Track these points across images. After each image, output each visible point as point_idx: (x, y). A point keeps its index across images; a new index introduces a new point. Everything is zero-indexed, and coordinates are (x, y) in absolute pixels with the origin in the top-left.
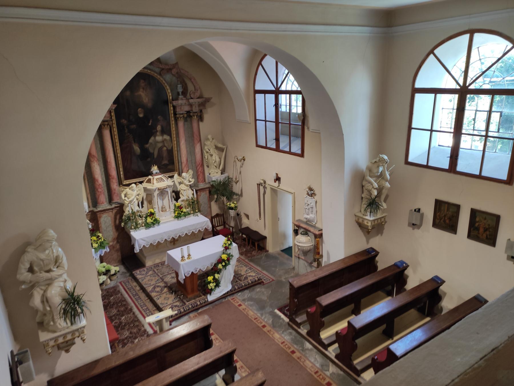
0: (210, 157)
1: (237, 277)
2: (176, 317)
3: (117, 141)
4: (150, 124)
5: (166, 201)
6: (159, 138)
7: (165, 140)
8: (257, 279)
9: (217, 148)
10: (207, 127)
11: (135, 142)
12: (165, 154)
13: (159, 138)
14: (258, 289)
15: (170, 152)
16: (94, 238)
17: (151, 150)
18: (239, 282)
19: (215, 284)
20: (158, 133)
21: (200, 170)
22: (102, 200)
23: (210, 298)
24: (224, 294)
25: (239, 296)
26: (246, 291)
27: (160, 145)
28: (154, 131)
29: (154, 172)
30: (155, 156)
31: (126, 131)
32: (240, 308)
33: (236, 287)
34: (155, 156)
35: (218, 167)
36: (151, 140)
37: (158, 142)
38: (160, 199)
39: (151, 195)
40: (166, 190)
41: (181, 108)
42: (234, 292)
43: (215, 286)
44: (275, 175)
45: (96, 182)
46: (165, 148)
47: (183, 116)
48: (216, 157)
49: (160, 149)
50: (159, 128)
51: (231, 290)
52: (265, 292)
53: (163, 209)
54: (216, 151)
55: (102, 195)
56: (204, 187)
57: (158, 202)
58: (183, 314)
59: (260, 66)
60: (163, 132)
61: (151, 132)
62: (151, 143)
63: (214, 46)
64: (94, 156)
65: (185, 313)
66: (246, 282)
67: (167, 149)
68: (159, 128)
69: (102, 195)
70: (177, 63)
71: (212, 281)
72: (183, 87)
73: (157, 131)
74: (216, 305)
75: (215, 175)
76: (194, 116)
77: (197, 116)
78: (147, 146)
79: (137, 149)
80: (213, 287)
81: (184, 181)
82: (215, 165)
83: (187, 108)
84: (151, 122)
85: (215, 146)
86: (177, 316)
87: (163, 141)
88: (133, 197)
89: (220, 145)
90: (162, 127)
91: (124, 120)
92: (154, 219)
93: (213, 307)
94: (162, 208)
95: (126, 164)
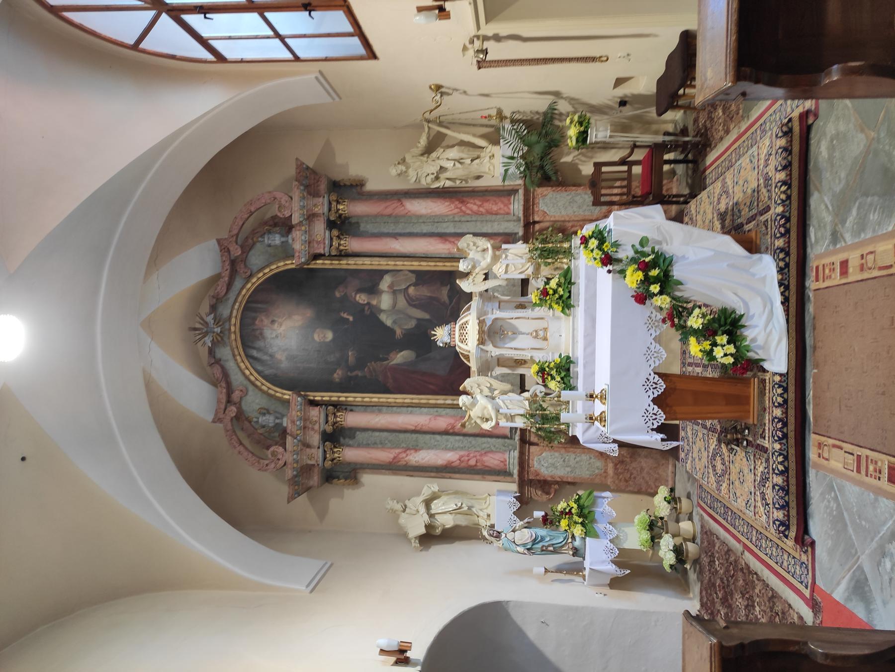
0: (448, 175)
1: (739, 228)
2: (793, 512)
3: (375, 398)
4: (351, 319)
5: (523, 326)
6: (385, 301)
7: (389, 287)
8: (782, 142)
9: (428, 151)
10: (376, 168)
11: (387, 359)
12: (425, 292)
13: (385, 301)
14: (821, 149)
15: (422, 277)
16: (564, 523)
17: (412, 324)
18: (767, 216)
19: (722, 339)
20: (374, 302)
21: (475, 208)
22: (496, 462)
23: (777, 360)
24: (785, 302)
25: (820, 250)
26: (814, 201)
27: (402, 302)
28: (367, 312)
29: (447, 339)
30: (427, 316)
31: (360, 374)
32: (854, 275)
33: (780, 243)
34: (427, 316)
35: (476, 153)
36: (387, 320)
37: (394, 305)
38: (513, 339)
39: (498, 359)
40: (489, 323)
41: (318, 243)
42: (793, 259)
43: (734, 338)
44: (421, 19)
45: (454, 464)
46: (411, 290)
47: (338, 237)
48: (447, 157)
49: (412, 302)
50: (362, 298)
51: (780, 271)
52: (842, 127)
53: (541, 335)
54: (434, 155)
55: (485, 459)
56: (522, 203)
57: (520, 346)
58: (793, 481)
59: (142, 46)
60: (372, 289)
61: (369, 317)
62: (394, 322)
63: (85, 194)
64: (395, 458)
65: (792, 473)
66: (778, 194)
67: (415, 285)
68: (362, 298)
69: (485, 459)
70: (219, 241)
71: (707, 345)
72: (269, 232)
73: (368, 304)
74: (815, 348)
75: (496, 165)
76: (338, 210)
77: (338, 202)
78: (399, 332)
79: (401, 357)
80: (731, 349)
81: (490, 264)
82: (468, 161)
83: (320, 228)
84: (345, 316)
85: (422, 155)
86: (793, 504)
87: (394, 293)
88: (490, 407)
89: (423, 141)
90: (360, 290)
91: (335, 375)
92: (554, 372)
93: (816, 366)
94: (536, 337)
95: (431, 387)
